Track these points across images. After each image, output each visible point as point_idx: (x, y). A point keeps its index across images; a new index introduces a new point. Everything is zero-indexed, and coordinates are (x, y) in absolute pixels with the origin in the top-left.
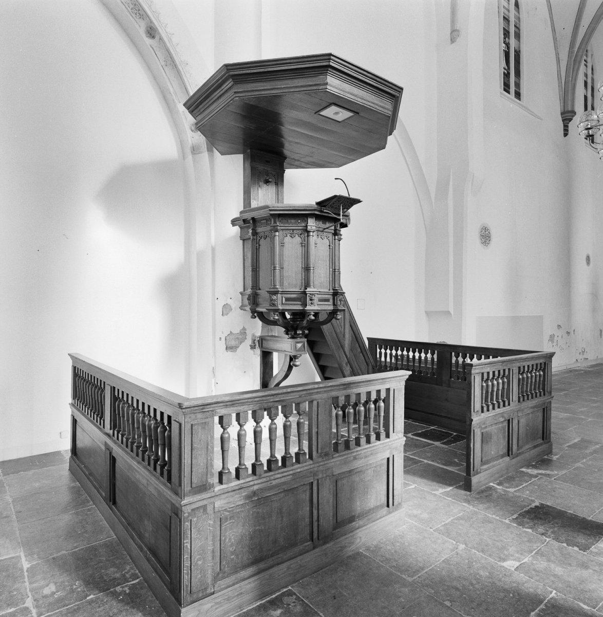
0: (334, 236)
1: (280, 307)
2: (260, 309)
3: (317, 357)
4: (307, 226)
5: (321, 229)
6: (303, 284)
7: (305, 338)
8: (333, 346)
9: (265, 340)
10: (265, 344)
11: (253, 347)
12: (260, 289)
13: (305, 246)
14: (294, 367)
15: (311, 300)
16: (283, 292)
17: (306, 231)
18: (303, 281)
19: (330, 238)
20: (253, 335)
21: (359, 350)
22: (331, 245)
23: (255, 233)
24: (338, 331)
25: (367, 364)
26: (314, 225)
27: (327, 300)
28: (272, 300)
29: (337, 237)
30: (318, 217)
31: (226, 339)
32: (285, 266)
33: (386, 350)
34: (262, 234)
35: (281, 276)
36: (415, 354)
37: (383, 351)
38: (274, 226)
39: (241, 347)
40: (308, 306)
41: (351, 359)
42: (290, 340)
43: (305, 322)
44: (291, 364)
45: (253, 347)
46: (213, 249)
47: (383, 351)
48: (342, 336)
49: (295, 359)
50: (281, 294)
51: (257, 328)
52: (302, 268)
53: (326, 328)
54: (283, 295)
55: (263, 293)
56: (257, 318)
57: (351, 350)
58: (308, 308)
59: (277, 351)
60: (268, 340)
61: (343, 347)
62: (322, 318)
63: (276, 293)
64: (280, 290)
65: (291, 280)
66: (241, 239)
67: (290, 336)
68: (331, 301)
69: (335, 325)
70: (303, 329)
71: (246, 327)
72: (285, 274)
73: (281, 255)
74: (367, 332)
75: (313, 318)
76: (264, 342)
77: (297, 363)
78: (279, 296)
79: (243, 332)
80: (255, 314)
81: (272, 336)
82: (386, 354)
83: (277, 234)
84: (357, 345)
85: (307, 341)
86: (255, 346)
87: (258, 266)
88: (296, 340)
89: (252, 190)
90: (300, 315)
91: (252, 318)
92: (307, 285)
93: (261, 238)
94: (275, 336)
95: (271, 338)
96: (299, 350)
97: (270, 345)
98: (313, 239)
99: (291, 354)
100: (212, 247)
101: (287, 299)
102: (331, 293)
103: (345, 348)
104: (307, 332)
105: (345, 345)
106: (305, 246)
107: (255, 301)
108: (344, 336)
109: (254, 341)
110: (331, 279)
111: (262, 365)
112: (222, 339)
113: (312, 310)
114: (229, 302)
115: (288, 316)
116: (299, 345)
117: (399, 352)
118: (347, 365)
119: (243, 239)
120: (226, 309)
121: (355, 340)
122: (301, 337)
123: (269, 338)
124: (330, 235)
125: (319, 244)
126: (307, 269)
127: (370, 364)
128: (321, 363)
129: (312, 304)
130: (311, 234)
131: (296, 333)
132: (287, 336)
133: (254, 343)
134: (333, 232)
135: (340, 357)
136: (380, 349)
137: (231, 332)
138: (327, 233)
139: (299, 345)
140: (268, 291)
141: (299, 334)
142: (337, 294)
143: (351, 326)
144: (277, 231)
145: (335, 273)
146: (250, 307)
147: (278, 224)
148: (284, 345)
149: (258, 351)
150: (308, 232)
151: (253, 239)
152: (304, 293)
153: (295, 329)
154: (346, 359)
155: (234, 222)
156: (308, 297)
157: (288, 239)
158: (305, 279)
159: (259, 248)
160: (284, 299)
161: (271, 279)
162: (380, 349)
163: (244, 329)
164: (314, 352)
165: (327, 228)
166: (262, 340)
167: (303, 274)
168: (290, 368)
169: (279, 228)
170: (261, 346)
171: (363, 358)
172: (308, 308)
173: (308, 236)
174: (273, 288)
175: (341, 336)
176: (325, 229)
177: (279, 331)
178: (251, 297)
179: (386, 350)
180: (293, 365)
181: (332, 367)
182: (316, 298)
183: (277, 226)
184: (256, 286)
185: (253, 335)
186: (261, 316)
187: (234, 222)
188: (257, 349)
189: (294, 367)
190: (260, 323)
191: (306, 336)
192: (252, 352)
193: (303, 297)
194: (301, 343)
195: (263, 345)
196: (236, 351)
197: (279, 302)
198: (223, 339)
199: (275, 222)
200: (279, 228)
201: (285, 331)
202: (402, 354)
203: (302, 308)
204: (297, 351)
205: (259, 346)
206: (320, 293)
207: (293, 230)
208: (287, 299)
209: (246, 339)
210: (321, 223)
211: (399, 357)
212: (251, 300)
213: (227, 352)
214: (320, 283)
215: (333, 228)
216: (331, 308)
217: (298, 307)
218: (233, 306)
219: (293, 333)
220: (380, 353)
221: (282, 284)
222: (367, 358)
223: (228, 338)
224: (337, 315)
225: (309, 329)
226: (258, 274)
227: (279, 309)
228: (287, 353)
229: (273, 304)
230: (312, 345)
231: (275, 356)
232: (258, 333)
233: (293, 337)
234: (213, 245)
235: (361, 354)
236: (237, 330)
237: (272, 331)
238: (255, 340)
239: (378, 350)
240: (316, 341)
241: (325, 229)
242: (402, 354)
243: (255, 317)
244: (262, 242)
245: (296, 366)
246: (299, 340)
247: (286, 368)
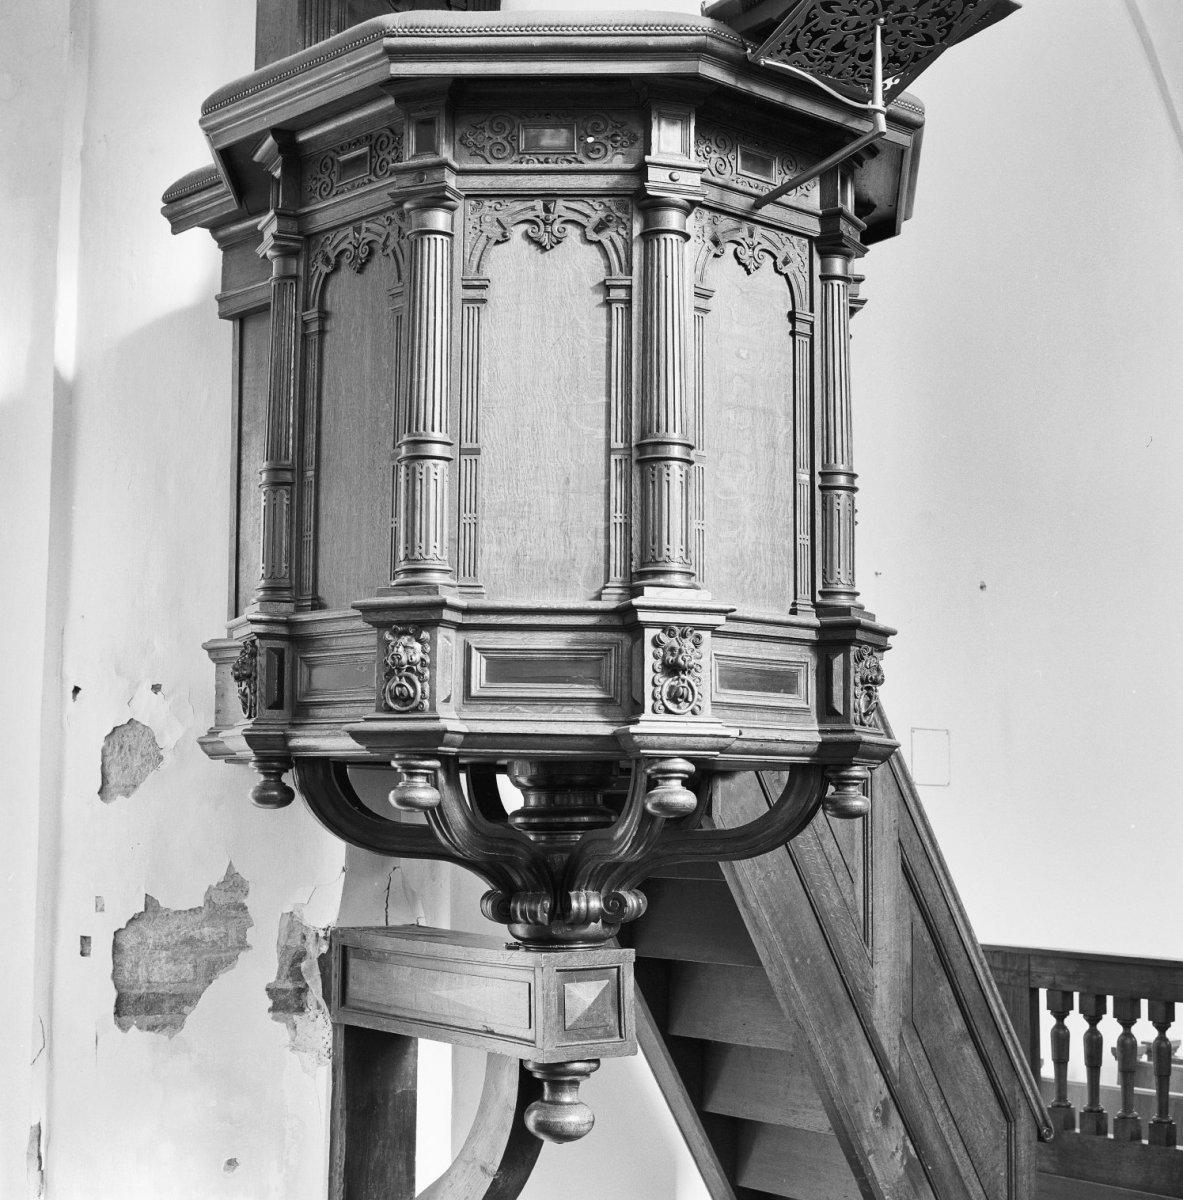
0: (825, 255)
1: (453, 719)
2: (328, 741)
3: (695, 1066)
4: (641, 171)
5: (739, 203)
6: (617, 561)
7: (624, 941)
8: (800, 998)
9: (365, 954)
10: (365, 983)
11: (287, 1002)
12: (318, 604)
13: (635, 308)
14: (549, 1146)
15: (672, 669)
16: (477, 619)
17: (639, 202)
18: (616, 544)
19: (798, 268)
20: (292, 923)
21: (957, 1023)
22: (803, 311)
23: (299, 242)
24: (831, 901)
25: (1008, 1115)
26: (694, 162)
27: (780, 680)
28: (392, 670)
29: (837, 265)
30: (722, 117)
31: (116, 948)
32: (490, 438)
33: (1094, 1018)
34: (345, 240)
35: (465, 504)
36: (1067, 1022)
37: (1076, 1024)
38: (421, 170)
39: (213, 996)
40: (648, 714)
41: (911, 1080)
42: (523, 957)
43: (625, 829)
44: (531, 1122)
45: (287, 1002)
46: (66, 395)
47: (1076, 1024)
48: (856, 935)
49: (557, 1086)
50: (461, 627)
51: (313, 876)
52: (609, 451)
53: (754, 881)
54: (476, 639)
55: (338, 619)
56: (299, 805)
57: (913, 1022)
58: (650, 725)
59: (439, 1028)
60: (381, 958)
61: (857, 1003)
62: (737, 804)
63: (423, 618)
64: (451, 600)
65: (520, 519)
66: (222, 316)
67: (520, 930)
68: (808, 683)
69: (812, 859)
70: (608, 877)
71: (244, 871)
72: (493, 493)
73: (468, 364)
74: (1002, 911)
75: (685, 798)
76: (353, 962)
77: (571, 1119)
78: (448, 642)
79: (229, 902)
80: (290, 779)
81: (415, 932)
82: (1094, 1043)
83: (439, 219)
84: (945, 989)
85: (640, 966)
86: (302, 991)
87: (311, 454)
88: (560, 958)
89: (707, 1110)
90: (591, 780)
91: (263, 799)
92: (643, 565)
93: (337, 268)
94: (433, 934)
95: (405, 945)
96: (585, 1028)
97: (396, 989)
98: (686, 257)
99: (525, 1052)
100: (58, 379)
101: (504, 667)
102: (811, 635)
103: (876, 1013)
104: (634, 902)
105: (870, 990)
106: (629, 302)
107: (298, 708)
108: (866, 936)
109: (293, 963)
110: (804, 538)
111: (342, 1133)
112: (94, 946)
113: (679, 744)
114: (149, 710)
115: (511, 797)
116: (584, 995)
117: (1144, 1031)
118: (885, 1119)
119: (239, 305)
120: (127, 755)
121: (932, 957)
122: (595, 940)
123: (388, 944)
124: (797, 251)
125: (728, 311)
126: (643, 457)
127: (1023, 1112)
128: (722, 1104)
129: (675, 696)
130: (673, 219)
131: (561, 910)
132: (502, 929)
133: (296, 974)
134: (814, 227)
135: (842, 1069)
136: (1060, 1014)
137: (149, 901)
138: (771, 234)
139: (584, 995)
140: (366, 610)
141: (587, 918)
142: (842, 637)
143: (907, 871)
144: (439, 199)
145: (825, 490)
146: (249, 723)
147: (446, 153)
148: (488, 995)
149: (319, 1029)
150: (650, 206)
151: (285, 278)
152: (625, 622)
153: (560, 885)
154: (878, 1078)
155: (180, 205)
156: (649, 649)
157: (512, 264)
158: (627, 527)
159: (322, 332)
160: (479, 664)
161: (394, 531)
162: (1060, 1014)
163: (233, 882)
164: (679, 1030)
165: (772, 198)
166: (344, 954)
167: (617, 491)
168: (521, 1151)
169: (452, 181)
170: (339, 994)
171: (980, 1075)
172: (650, 725)
173: (651, 235)
174: (405, 587)
175: (848, 937)
176: (760, 202)
177: (452, 894)
178: (261, 660)
179: (1094, 1018)
180: (544, 1127)
181: (786, 1131)
182: (706, 657)
183: (444, 165)
184: (294, 578)
185: (292, 923)
186: (336, 796)
187: (180, 205)
188: (311, 1011)
189: (549, 1146)
190: (335, 849)
191: (628, 933)
192: (279, 1030)
193: (617, 642)
194: (597, 980)
195: (352, 987)
196: (176, 1025)
197: (447, 681)
198: (102, 948)
199: (427, 145)
200: (452, 181)
201: (487, 896)
202: (1162, 1037)
203: (607, 730)
204: (567, 1032)
205: (327, 996)
206: (732, 625)
207: (549, 196)
208: (504, 667)
209: (243, 945)
210: (736, 160)
211: (1144, 1058)
212: (262, 677)
213: (123, 1027)
214: (729, 553)
215: (811, 197)
216: (807, 732)
217: (580, 720)
218: (167, 741)
219: (543, 908)
220: (1061, 1040)
221: (466, 559)
222: (1002, 1075)
223: (129, 941)
224: (842, 783)
225: (646, 887)
226: (309, 506)
227: (439, 735)
228: (500, 1047)
229: (395, 698)
230: (663, 987)
231: (433, 1068)
232: (324, 912)
233: (541, 940)
234: (68, 370)
235: (969, 1051)
236: (186, 892)
237: (411, 898)
238: (301, 956)
239: (1047, 1021)
240: (411, 1037)
241: (760, 202)
242: (1162, 1037)
243: (286, 797)
244: (345, 293)
245: (562, 1136)
246: (579, 957)
247: (494, 1148)
